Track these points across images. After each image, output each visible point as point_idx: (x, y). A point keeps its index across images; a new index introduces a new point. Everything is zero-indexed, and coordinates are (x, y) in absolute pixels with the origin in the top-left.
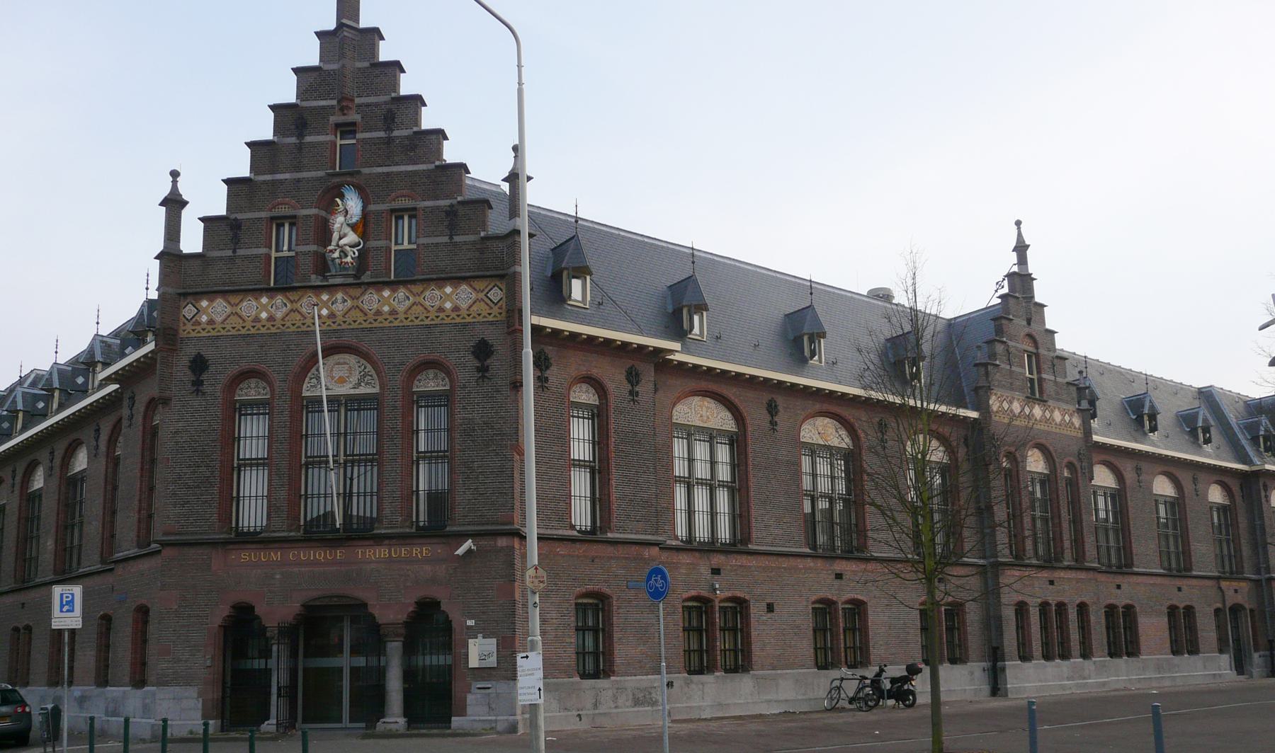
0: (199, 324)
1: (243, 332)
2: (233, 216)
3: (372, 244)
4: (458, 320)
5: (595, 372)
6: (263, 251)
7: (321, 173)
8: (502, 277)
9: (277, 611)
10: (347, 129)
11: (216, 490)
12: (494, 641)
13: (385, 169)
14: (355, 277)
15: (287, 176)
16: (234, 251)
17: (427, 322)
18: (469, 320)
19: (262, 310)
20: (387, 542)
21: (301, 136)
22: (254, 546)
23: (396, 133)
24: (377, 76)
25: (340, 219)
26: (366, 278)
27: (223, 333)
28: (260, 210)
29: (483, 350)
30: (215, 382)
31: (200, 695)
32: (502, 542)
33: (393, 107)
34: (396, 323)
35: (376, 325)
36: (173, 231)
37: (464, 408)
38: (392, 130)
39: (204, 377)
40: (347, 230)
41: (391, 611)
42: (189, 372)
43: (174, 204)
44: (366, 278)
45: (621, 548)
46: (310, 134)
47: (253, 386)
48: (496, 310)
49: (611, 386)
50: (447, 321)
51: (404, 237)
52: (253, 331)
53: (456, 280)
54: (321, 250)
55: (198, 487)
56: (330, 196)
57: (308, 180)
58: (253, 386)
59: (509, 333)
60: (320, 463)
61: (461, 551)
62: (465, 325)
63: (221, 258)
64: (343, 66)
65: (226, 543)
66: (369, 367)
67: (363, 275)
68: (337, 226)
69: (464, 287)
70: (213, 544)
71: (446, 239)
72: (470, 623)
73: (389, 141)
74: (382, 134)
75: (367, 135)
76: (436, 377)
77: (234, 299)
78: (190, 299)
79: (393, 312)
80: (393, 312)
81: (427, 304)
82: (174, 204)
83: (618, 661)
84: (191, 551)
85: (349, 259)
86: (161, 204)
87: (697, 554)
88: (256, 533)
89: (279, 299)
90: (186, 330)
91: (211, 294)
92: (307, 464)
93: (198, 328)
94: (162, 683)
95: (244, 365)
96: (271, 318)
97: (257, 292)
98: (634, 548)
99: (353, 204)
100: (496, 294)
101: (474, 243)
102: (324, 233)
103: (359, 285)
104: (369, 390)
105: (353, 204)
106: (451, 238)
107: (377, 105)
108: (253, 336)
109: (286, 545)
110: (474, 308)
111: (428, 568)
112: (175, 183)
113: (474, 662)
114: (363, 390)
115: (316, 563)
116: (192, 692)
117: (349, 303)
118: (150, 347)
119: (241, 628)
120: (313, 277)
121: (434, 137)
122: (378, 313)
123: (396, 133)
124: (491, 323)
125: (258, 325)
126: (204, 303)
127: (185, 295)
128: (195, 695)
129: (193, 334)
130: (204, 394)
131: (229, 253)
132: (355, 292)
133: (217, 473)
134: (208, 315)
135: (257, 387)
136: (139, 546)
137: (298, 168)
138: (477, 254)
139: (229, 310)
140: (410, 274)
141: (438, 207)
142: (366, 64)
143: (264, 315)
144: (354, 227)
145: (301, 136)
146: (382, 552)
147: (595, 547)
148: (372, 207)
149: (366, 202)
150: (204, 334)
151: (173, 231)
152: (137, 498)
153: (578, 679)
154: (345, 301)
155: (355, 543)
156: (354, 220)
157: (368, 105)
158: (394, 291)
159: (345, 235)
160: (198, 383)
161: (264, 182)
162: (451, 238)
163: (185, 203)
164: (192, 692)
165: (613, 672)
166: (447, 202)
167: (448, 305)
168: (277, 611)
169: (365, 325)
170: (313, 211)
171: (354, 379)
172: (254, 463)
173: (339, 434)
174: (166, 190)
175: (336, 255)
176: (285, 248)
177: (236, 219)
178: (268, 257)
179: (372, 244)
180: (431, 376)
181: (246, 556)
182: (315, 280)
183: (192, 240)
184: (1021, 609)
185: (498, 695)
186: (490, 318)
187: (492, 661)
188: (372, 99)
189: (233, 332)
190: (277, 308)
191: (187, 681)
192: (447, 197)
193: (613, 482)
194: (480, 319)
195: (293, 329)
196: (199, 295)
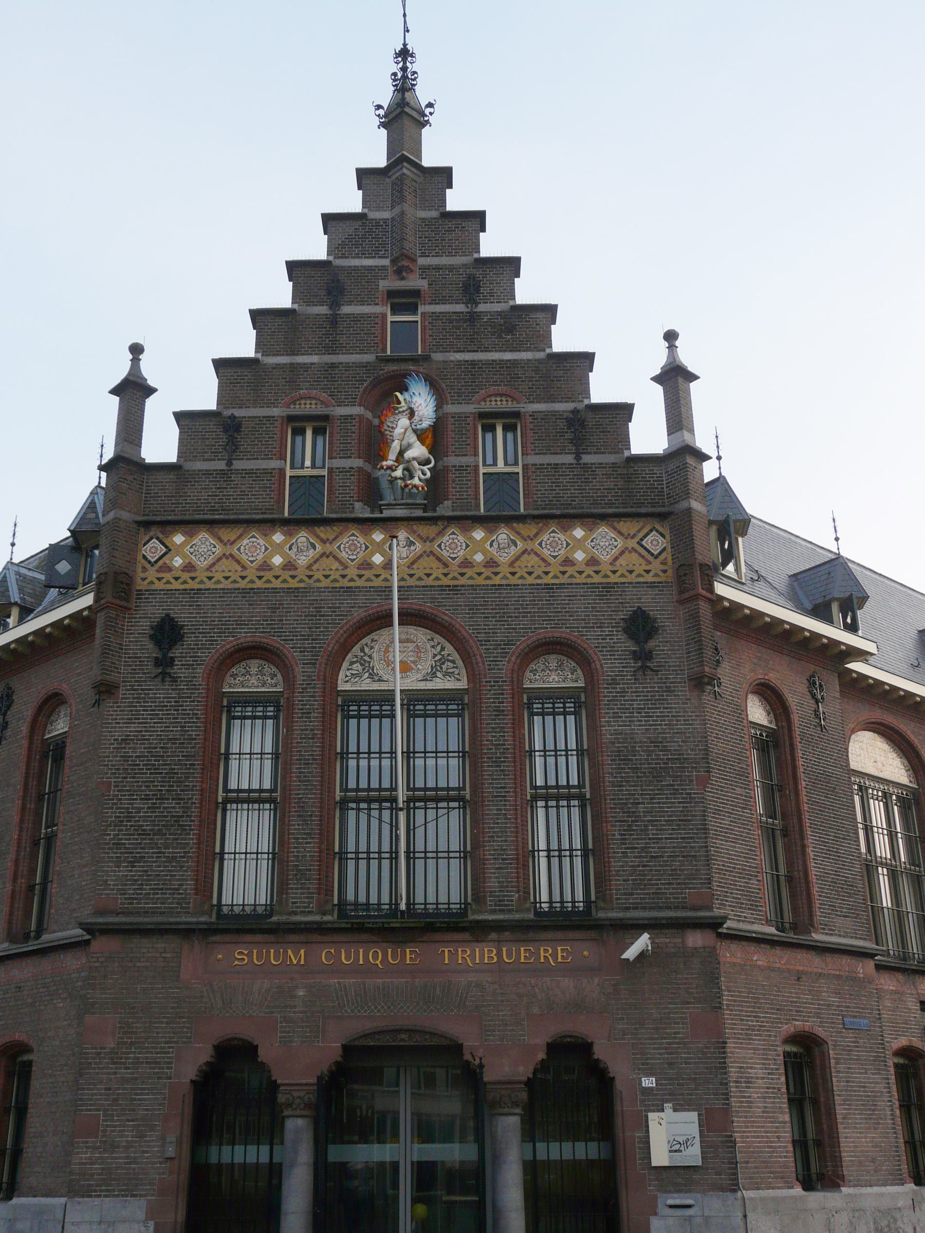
0: (169, 569)
1: (243, 584)
2: (227, 413)
3: (452, 460)
4: (597, 579)
5: (773, 678)
6: (274, 464)
7: (369, 358)
8: (662, 517)
9: (298, 1059)
10: (405, 301)
11: (192, 839)
12: (693, 1116)
13: (468, 356)
14: (425, 508)
15: (315, 359)
16: (229, 463)
17: (548, 580)
18: (613, 579)
19: (274, 552)
20: (494, 936)
21: (335, 304)
22: (259, 938)
23: (482, 308)
24: (450, 231)
25: (404, 422)
26: (445, 509)
27: (209, 585)
28: (270, 405)
29: (640, 626)
30: (193, 661)
31: (151, 1214)
32: (695, 939)
33: (478, 273)
34: (497, 580)
35: (463, 581)
36: (130, 427)
37: (616, 716)
38: (477, 304)
39: (176, 652)
40: (413, 438)
41: (509, 1061)
42: (150, 646)
43: (133, 391)
44: (445, 509)
45: (829, 958)
46: (350, 303)
47: (254, 670)
48: (656, 566)
49: (792, 700)
50: (580, 579)
51: (498, 454)
52: (259, 584)
53: (591, 519)
54: (368, 467)
55: (160, 832)
56: (386, 389)
57: (348, 366)
58: (254, 670)
59: (681, 602)
60: (380, 800)
61: (631, 953)
62: (609, 587)
63: (208, 473)
64: (403, 213)
65: (207, 932)
66: (449, 649)
67: (436, 506)
68: (398, 431)
69: (603, 529)
70: (186, 932)
71: (569, 459)
72: (648, 1082)
73: (472, 318)
74: (460, 308)
75: (439, 308)
76: (560, 666)
77: (228, 534)
78: (154, 531)
79: (491, 563)
80: (491, 563)
81: (546, 553)
82: (133, 391)
83: (847, 1157)
84: (147, 947)
85: (416, 481)
86: (114, 391)
87: (900, 977)
88: (254, 916)
89: (303, 537)
90: (145, 579)
91: (189, 525)
92: (344, 802)
93: (167, 576)
94: (77, 1189)
95: (245, 637)
96: (289, 566)
97: (268, 523)
98: (845, 960)
99: (421, 401)
100: (655, 542)
101: (614, 466)
102: (374, 443)
103: (434, 520)
104: (450, 684)
105: (421, 401)
106: (578, 458)
107: (451, 268)
108: (258, 591)
109: (316, 937)
110: (622, 561)
111: (567, 983)
112: (135, 361)
113: (660, 1157)
114: (439, 684)
115: (369, 970)
116: (136, 1208)
117: (418, 547)
118: (87, 600)
119: (229, 1092)
120: (358, 505)
121: (540, 315)
122: (467, 563)
123: (482, 308)
124: (652, 585)
125: (268, 575)
126: (179, 539)
127: (147, 525)
128: (141, 1215)
129: (158, 585)
130: (174, 680)
131: (221, 465)
132: (431, 530)
133: (195, 811)
134: (184, 556)
135: (261, 672)
136: (11, 938)
137: (331, 349)
138: (621, 483)
139: (219, 550)
140: (501, 511)
141: (554, 413)
142: (434, 214)
143: (277, 560)
144: (421, 436)
145: (335, 304)
146: (484, 954)
147: (801, 955)
148: (450, 408)
149: (440, 405)
150: (176, 585)
151: (130, 427)
152: (12, 856)
153: (798, 1191)
154: (412, 543)
155: (438, 936)
156: (426, 424)
157: (437, 268)
158: (491, 531)
159: (409, 446)
160: (164, 663)
161: (277, 366)
162: (578, 458)
163: (151, 391)
164: (136, 1208)
165: (843, 1178)
166: (570, 406)
167: (580, 556)
168: (298, 1059)
169: (445, 581)
170: (356, 410)
171: (425, 666)
172: (554, 795)
173: (408, 752)
174: (121, 372)
175: (399, 473)
176: (308, 463)
177: (233, 417)
178: (282, 471)
179: (452, 460)
180: (553, 665)
181: (243, 955)
182: (361, 510)
183: (160, 444)
184: (805, 1062)
185: (707, 1219)
186: (649, 578)
187: (693, 1155)
188: (444, 261)
189: (226, 584)
190: (300, 551)
191: (127, 1187)
192: (568, 399)
193: (810, 850)
194: (632, 578)
195: (325, 583)
196: (169, 525)
